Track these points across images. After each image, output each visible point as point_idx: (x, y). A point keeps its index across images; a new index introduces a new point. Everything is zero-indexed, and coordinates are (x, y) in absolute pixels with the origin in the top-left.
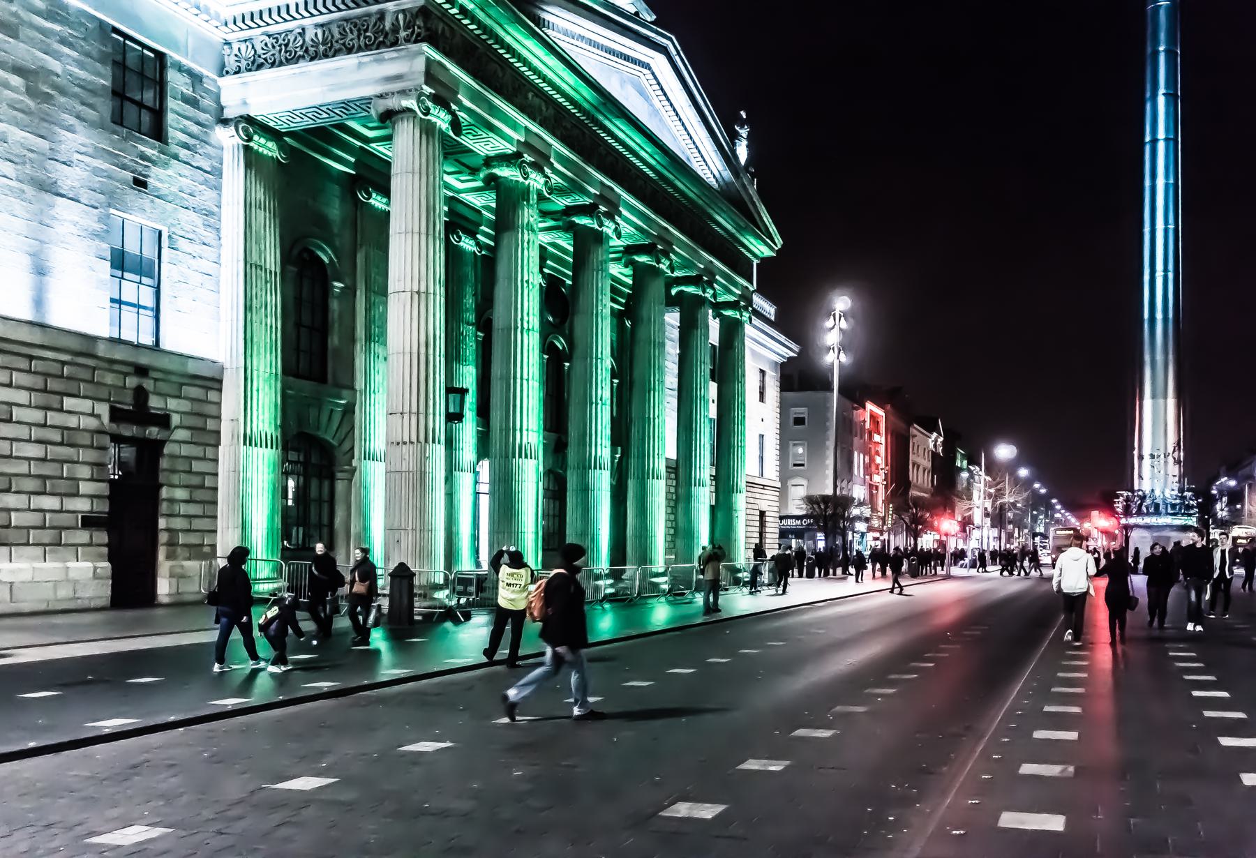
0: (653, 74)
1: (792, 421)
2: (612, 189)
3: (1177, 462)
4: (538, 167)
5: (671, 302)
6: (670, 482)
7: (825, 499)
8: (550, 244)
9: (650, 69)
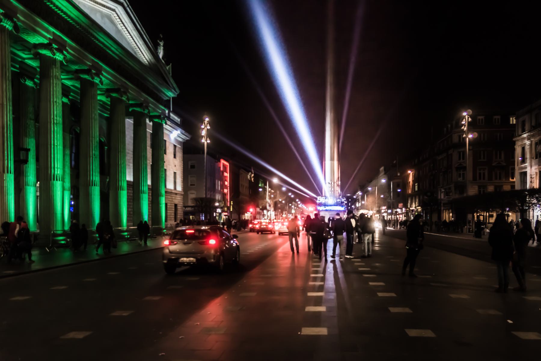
0: (117, 14)
1: (189, 167)
2: (98, 63)
3: (338, 185)
4: (60, 51)
5: (129, 115)
6: (130, 191)
7: (202, 199)
8: (72, 86)
9: (115, 12)
